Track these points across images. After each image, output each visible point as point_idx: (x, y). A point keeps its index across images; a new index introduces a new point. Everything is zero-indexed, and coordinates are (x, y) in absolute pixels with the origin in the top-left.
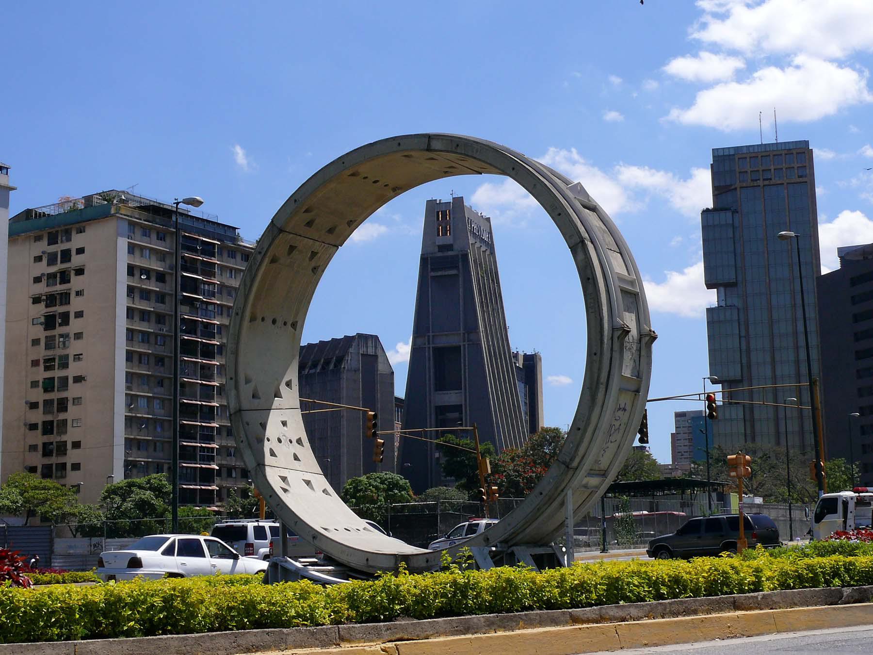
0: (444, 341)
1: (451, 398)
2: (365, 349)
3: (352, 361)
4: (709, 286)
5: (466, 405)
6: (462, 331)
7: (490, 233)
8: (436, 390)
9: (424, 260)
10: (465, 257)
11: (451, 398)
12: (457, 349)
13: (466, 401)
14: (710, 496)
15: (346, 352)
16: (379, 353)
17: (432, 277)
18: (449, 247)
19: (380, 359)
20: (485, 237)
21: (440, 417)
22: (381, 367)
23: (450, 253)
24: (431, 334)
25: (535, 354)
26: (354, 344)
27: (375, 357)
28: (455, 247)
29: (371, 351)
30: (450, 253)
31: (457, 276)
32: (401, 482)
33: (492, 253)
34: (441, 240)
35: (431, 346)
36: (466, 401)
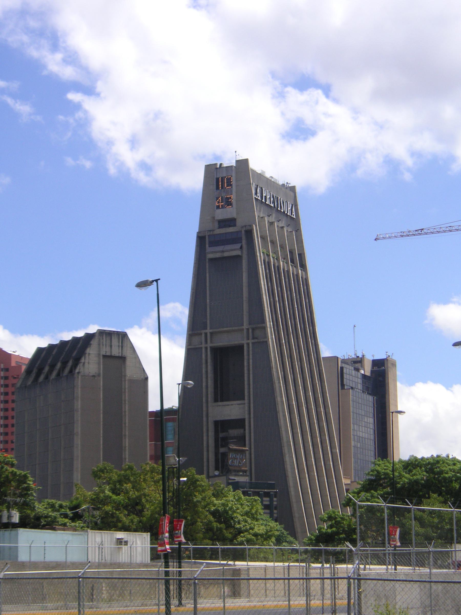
0: (224, 341)
1: (231, 410)
2: (108, 349)
3: (91, 364)
4: (237, 162)
5: (250, 418)
6: (245, 326)
7: (295, 205)
8: (216, 400)
9: (201, 240)
10: (249, 233)
11: (231, 410)
12: (239, 349)
13: (250, 414)
14: (455, 560)
15: (82, 353)
16: (127, 353)
17: (211, 260)
18: (231, 222)
19: (129, 362)
20: (287, 209)
21: (221, 435)
22: (130, 372)
23: (231, 230)
24: (208, 331)
25: (386, 359)
26: (94, 343)
27: (123, 359)
28: (239, 223)
29: (116, 352)
30: (231, 230)
31: (238, 258)
32: (255, 510)
33: (298, 230)
34: (221, 214)
35: (209, 345)
36: (250, 414)
